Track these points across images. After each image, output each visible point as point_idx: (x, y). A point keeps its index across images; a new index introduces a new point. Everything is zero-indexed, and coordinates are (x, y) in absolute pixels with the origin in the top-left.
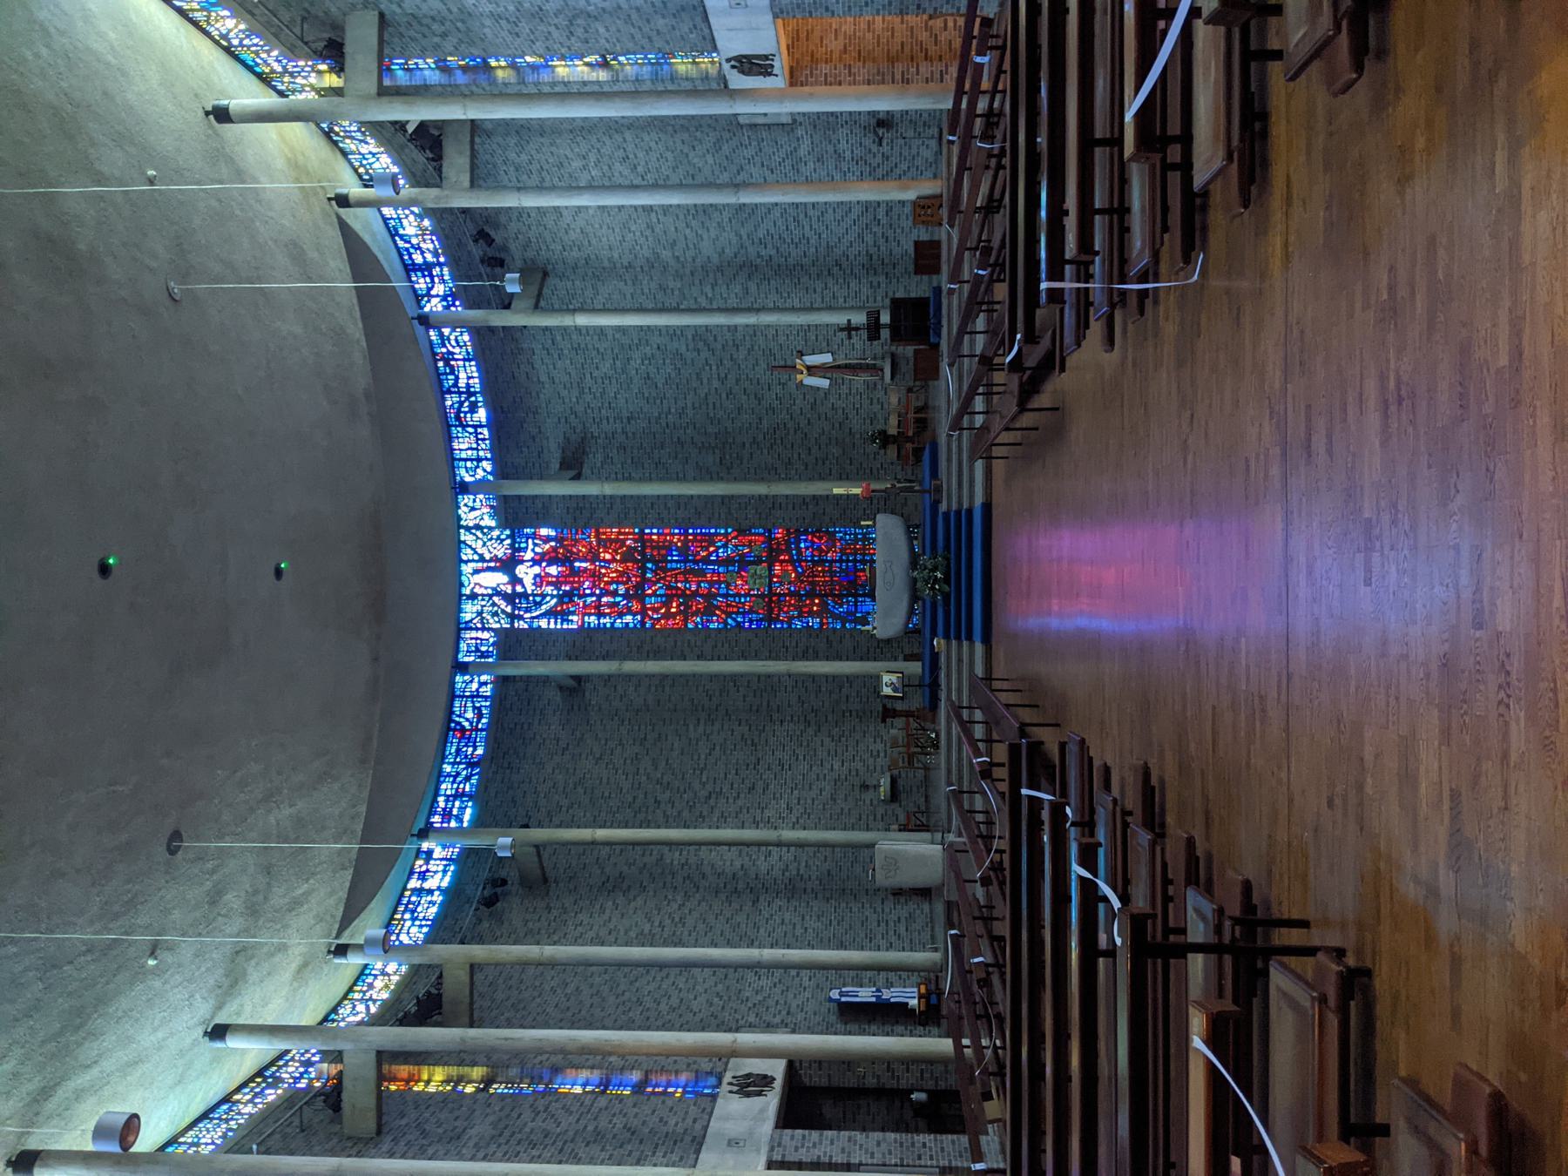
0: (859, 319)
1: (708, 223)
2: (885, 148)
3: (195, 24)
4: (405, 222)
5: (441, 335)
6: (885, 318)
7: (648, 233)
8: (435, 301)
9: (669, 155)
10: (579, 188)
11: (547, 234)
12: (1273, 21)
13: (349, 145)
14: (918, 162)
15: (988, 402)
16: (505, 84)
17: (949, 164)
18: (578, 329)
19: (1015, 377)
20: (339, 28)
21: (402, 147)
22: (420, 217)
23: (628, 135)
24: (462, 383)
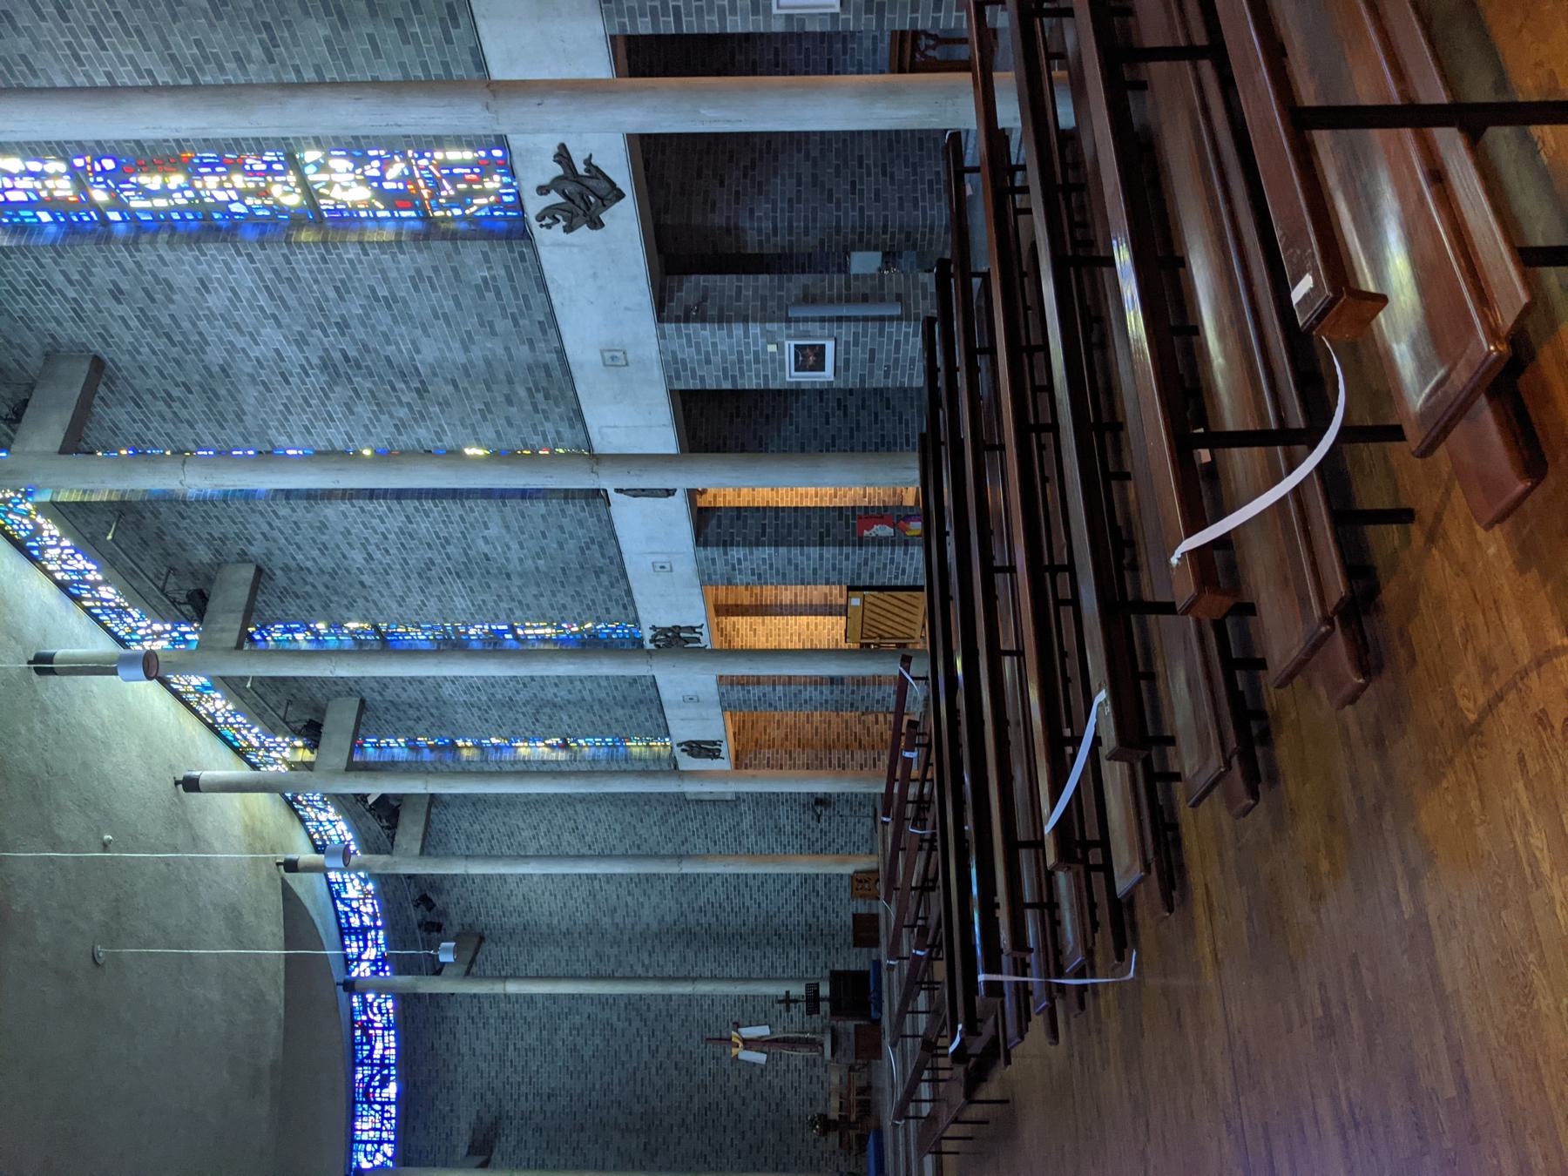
0: (798, 990)
1: (649, 892)
2: (823, 824)
3: (186, 704)
4: (349, 886)
5: (364, 1001)
6: (825, 990)
7: (590, 900)
8: (364, 965)
9: (618, 827)
10: (526, 857)
11: (489, 900)
12: (1170, 750)
13: (310, 813)
14: (855, 838)
15: (935, 1090)
16: (469, 762)
17: (884, 842)
18: (507, 997)
19: (960, 1070)
20: (321, 711)
21: (360, 816)
22: (365, 881)
23: (579, 807)
24: (377, 1054)
